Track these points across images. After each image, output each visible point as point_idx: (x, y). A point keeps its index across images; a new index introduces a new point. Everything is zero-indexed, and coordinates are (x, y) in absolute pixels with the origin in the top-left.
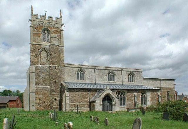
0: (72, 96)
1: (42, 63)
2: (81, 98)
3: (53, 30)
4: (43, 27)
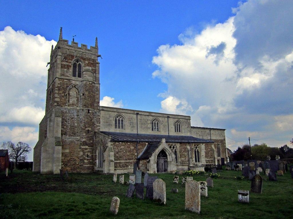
0: (117, 150)
1: (70, 104)
2: (128, 154)
3: (87, 62)
4: (75, 57)
